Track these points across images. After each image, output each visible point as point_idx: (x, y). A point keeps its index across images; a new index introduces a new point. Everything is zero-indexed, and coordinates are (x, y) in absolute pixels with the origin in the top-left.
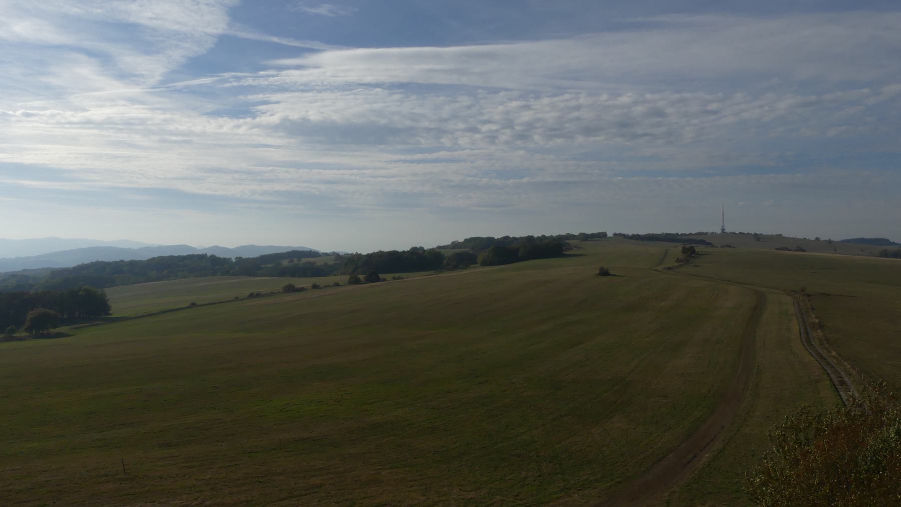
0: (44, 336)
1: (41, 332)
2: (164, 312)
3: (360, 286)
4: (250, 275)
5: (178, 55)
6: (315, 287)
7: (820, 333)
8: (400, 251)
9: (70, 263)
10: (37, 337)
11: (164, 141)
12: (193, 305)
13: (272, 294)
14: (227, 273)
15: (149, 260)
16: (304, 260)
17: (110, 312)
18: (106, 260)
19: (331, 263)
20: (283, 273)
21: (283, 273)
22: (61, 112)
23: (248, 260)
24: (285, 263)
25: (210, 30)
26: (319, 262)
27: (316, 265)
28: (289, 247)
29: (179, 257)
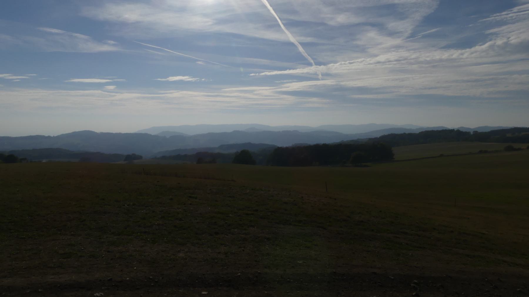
5: (418, 16)
7: (327, 267)
8: (153, 134)
9: (378, 135)
11: (434, 67)
12: (442, 155)
15: (420, 133)
22: (365, 59)
24: (509, 135)
29: (437, 131)
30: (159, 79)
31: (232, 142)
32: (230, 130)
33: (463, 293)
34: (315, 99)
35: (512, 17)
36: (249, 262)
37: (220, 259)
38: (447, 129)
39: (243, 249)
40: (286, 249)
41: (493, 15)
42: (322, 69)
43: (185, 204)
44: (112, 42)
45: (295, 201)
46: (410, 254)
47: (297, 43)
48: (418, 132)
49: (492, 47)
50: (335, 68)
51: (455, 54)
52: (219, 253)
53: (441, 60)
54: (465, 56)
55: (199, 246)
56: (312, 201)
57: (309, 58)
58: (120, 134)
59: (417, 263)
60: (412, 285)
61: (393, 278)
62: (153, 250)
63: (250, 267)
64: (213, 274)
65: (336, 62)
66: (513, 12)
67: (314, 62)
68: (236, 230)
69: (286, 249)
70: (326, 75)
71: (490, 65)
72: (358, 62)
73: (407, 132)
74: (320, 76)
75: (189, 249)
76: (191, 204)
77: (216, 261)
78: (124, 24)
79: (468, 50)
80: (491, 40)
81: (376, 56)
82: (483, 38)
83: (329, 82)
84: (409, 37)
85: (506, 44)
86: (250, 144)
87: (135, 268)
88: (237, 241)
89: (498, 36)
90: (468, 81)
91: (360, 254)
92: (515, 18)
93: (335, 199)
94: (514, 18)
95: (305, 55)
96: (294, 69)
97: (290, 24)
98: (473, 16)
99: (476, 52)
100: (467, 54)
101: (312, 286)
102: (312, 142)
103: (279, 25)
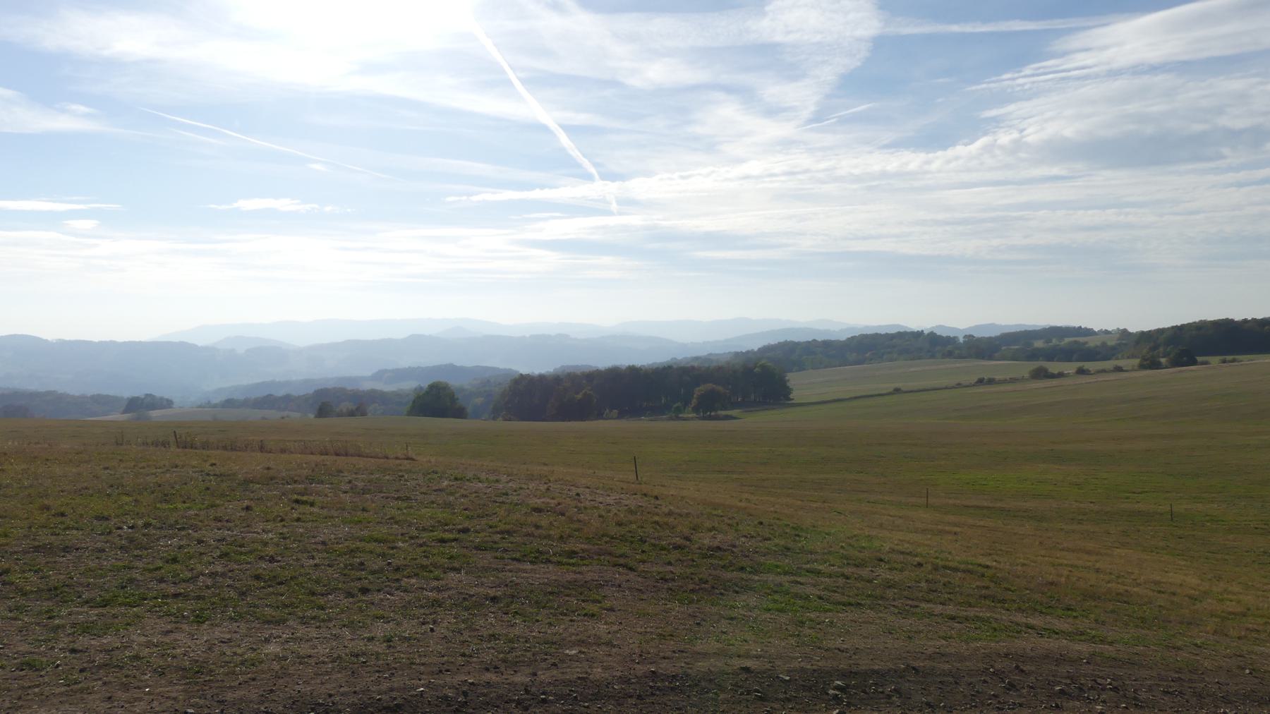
0: (711, 418)
1: (709, 413)
2: (856, 398)
3: (1159, 371)
4: (983, 358)
5: (828, 74)
6: (1081, 372)
8: (200, 345)
10: (704, 418)
13: (1013, 380)
14: (950, 354)
16: (1067, 340)
17: (791, 396)
18: (796, 340)
19: (1111, 343)
20: (1033, 355)
21: (1033, 355)
23: (980, 340)
24: (1039, 344)
25: (860, 32)
26: (1092, 342)
27: (1087, 346)
28: (992, 326)
30: (212, 206)
31: (406, 362)
32: (400, 334)
33: (942, 704)
34: (607, 260)
35: (1023, 85)
36: (446, 658)
37: (372, 655)
38: (908, 331)
39: (432, 626)
40: (537, 621)
41: (1020, 71)
42: (610, 189)
43: (282, 520)
44: (82, 109)
45: (559, 504)
46: (827, 620)
47: (556, 126)
48: (843, 338)
49: (988, 149)
50: (639, 187)
51: (913, 160)
52: (371, 639)
53: (884, 175)
54: (934, 166)
55: (318, 624)
56: (601, 503)
57: (586, 163)
58: (113, 343)
59: (843, 641)
60: (831, 692)
61: (788, 678)
62: (197, 639)
63: (448, 671)
64: (355, 692)
65: (648, 174)
66: (1023, 74)
67: (599, 173)
68: (413, 581)
69: (537, 621)
70: (628, 203)
71: (990, 189)
72: (700, 174)
73: (819, 339)
74: (614, 207)
75: (293, 634)
76: (298, 520)
77: (362, 659)
78: (114, 65)
79: (940, 153)
80: (985, 134)
81: (740, 161)
82: (967, 127)
83: (636, 220)
84: (810, 121)
85: (1017, 146)
86: (452, 369)
87: (147, 690)
88: (416, 607)
89: (1002, 125)
90: (946, 223)
91: (714, 627)
92: (1030, 89)
93: (656, 498)
94: (1026, 87)
95: (576, 154)
96: (551, 187)
97: (539, 82)
98: (941, 80)
99: (957, 158)
100: (938, 160)
101: (599, 708)
102: (603, 362)
103: (509, 83)
